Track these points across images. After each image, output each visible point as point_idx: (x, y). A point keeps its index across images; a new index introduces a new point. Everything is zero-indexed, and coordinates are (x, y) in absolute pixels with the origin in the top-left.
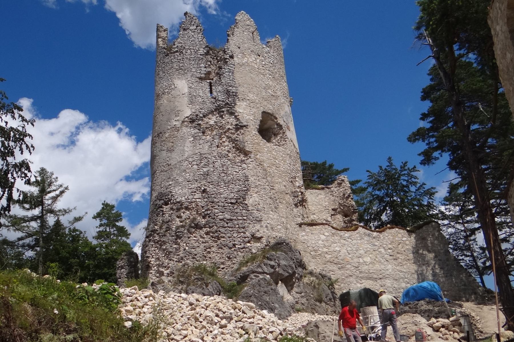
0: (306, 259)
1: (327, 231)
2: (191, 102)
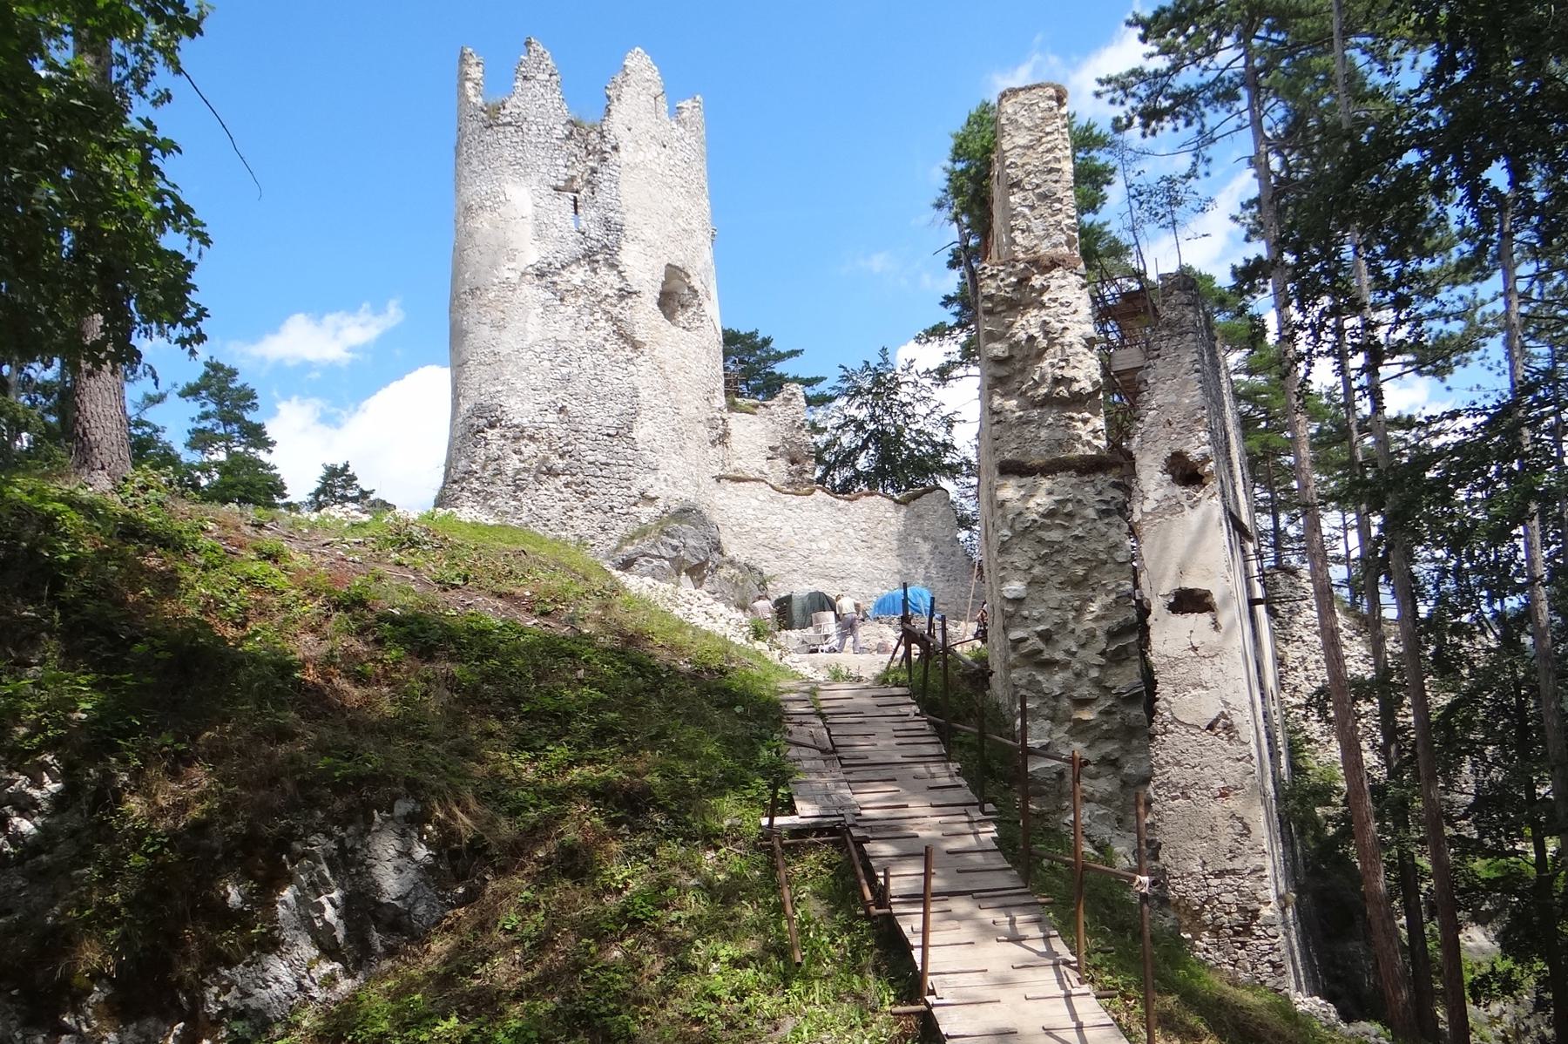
0: (725, 538)
1: (763, 491)
2: (540, 236)
